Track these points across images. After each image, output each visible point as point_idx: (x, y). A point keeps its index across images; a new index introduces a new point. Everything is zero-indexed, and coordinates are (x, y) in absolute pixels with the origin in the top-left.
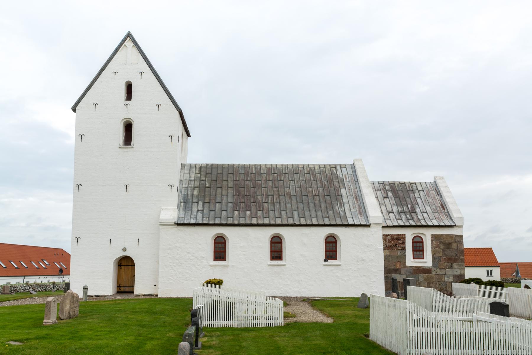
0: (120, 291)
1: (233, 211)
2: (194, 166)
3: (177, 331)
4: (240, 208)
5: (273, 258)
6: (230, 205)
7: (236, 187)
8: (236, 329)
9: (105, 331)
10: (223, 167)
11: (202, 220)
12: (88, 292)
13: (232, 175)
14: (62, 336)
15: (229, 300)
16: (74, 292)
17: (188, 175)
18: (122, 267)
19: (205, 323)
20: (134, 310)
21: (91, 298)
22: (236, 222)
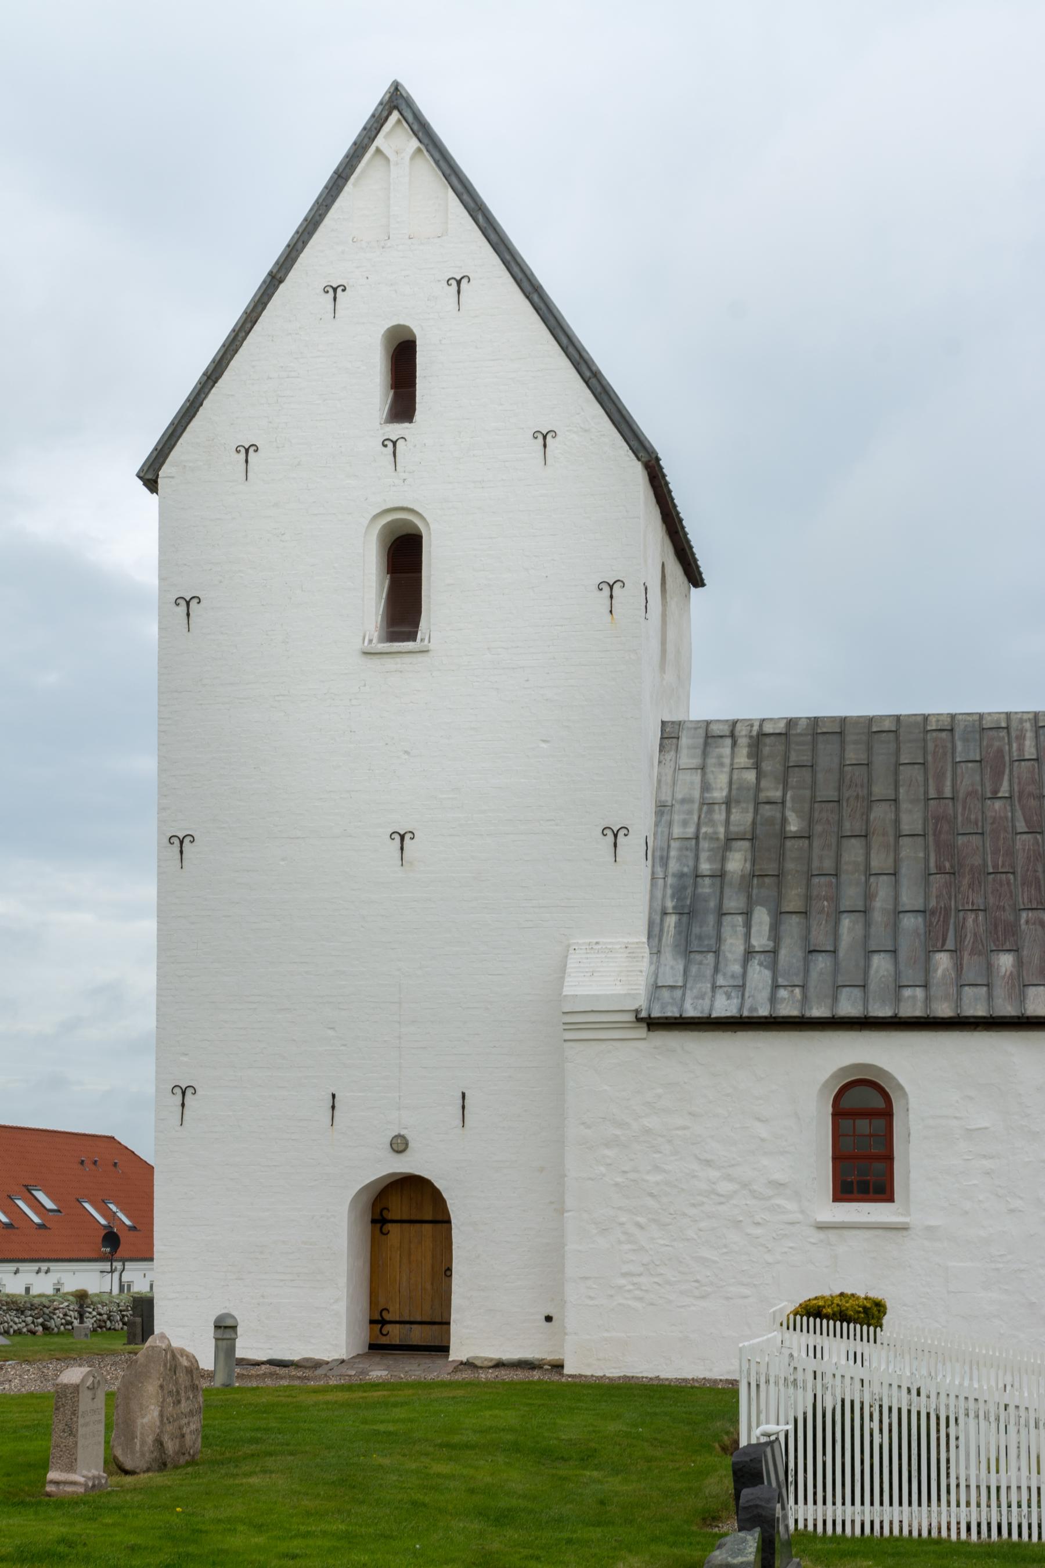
0: (384, 1341)
1: (929, 953)
2: (725, 730)
3: (664, 1549)
4: (960, 939)
5: (847, 1188)
6: (910, 923)
7: (940, 833)
8: (960, 1550)
9: (324, 1533)
10: (870, 730)
11: (773, 999)
12: (239, 1343)
13: (917, 773)
14: (133, 1549)
15: (921, 1404)
16: (175, 1344)
17: (697, 778)
18: (390, 1227)
19: (801, 1514)
20: (456, 1439)
21: (253, 1371)
22: (944, 1010)
